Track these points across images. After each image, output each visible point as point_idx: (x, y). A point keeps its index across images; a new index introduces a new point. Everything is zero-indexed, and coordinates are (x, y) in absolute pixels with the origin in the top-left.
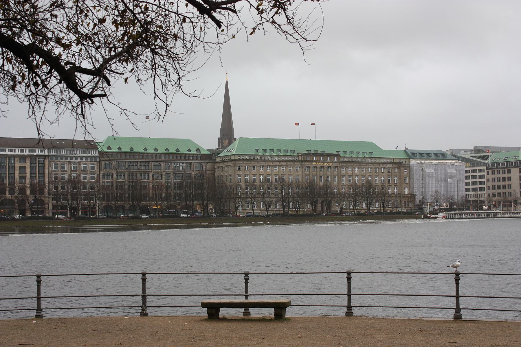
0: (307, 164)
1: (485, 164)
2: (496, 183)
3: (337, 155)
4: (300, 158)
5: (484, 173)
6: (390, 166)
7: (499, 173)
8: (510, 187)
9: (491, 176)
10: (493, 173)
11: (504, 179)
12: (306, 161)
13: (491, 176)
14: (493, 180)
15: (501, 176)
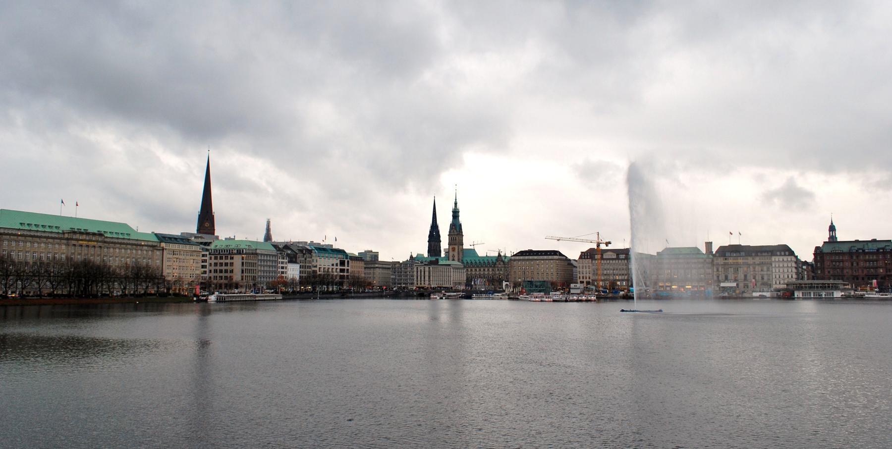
0: (74, 242)
1: (207, 250)
2: (218, 268)
3: (100, 235)
4: (66, 236)
5: (207, 258)
6: (146, 248)
7: (221, 258)
8: (232, 271)
9: (213, 261)
10: (216, 258)
11: (226, 264)
12: (72, 239)
13: (213, 261)
14: (216, 264)
15: (223, 261)
